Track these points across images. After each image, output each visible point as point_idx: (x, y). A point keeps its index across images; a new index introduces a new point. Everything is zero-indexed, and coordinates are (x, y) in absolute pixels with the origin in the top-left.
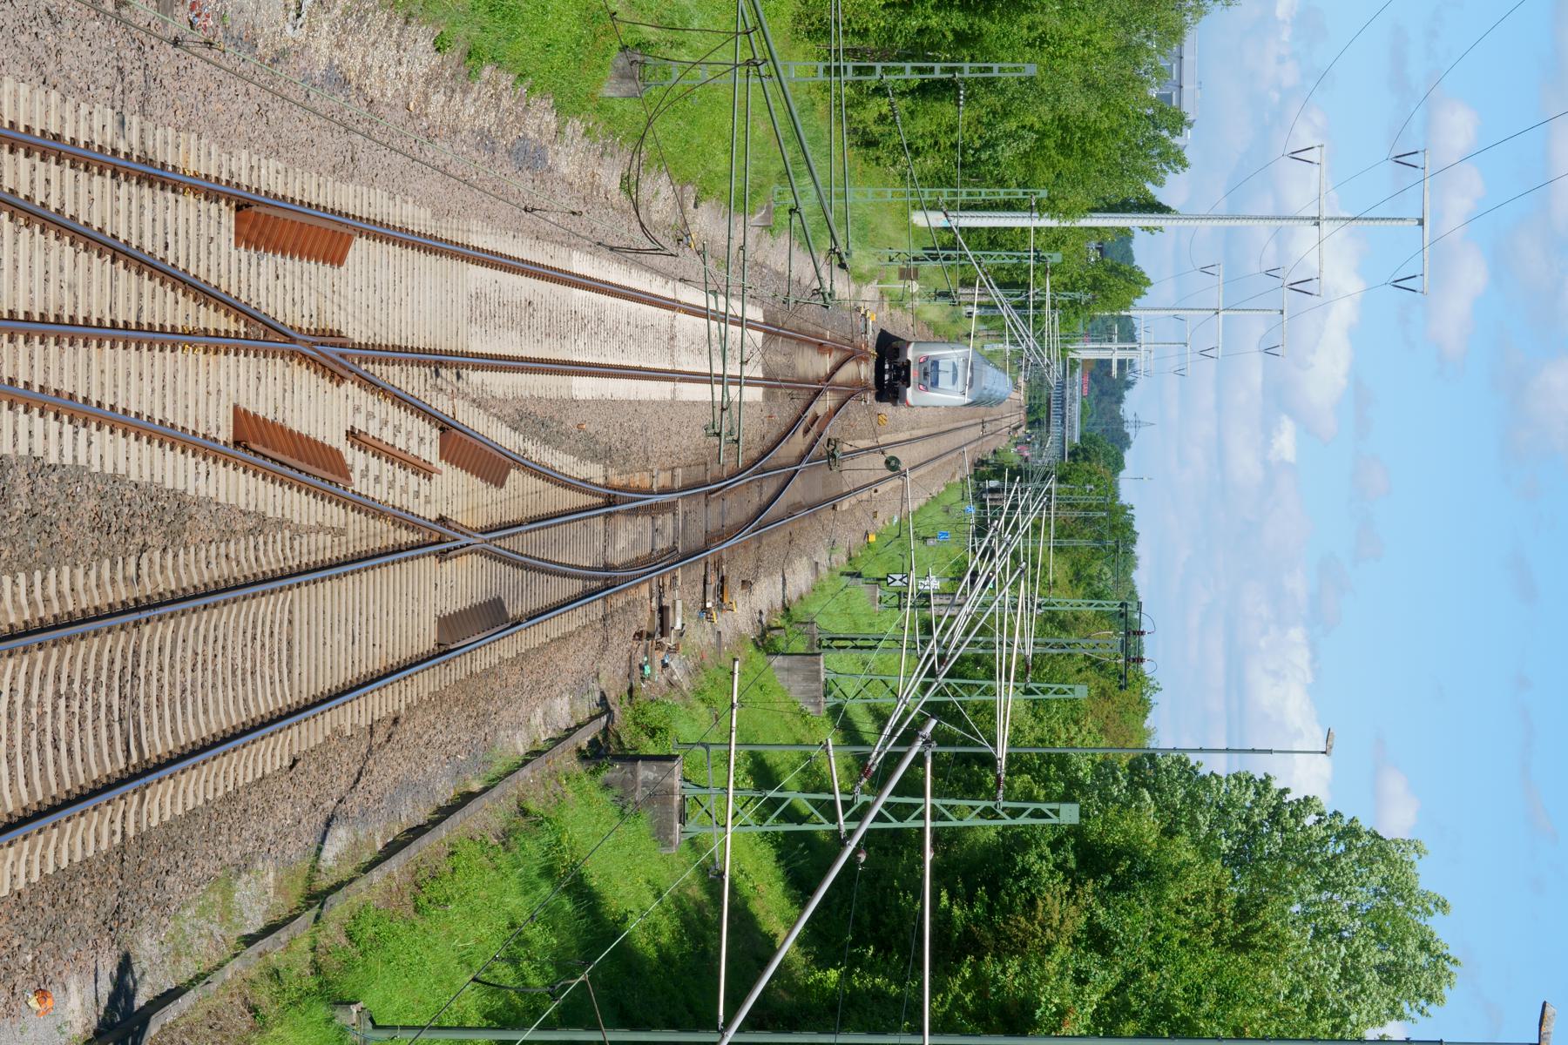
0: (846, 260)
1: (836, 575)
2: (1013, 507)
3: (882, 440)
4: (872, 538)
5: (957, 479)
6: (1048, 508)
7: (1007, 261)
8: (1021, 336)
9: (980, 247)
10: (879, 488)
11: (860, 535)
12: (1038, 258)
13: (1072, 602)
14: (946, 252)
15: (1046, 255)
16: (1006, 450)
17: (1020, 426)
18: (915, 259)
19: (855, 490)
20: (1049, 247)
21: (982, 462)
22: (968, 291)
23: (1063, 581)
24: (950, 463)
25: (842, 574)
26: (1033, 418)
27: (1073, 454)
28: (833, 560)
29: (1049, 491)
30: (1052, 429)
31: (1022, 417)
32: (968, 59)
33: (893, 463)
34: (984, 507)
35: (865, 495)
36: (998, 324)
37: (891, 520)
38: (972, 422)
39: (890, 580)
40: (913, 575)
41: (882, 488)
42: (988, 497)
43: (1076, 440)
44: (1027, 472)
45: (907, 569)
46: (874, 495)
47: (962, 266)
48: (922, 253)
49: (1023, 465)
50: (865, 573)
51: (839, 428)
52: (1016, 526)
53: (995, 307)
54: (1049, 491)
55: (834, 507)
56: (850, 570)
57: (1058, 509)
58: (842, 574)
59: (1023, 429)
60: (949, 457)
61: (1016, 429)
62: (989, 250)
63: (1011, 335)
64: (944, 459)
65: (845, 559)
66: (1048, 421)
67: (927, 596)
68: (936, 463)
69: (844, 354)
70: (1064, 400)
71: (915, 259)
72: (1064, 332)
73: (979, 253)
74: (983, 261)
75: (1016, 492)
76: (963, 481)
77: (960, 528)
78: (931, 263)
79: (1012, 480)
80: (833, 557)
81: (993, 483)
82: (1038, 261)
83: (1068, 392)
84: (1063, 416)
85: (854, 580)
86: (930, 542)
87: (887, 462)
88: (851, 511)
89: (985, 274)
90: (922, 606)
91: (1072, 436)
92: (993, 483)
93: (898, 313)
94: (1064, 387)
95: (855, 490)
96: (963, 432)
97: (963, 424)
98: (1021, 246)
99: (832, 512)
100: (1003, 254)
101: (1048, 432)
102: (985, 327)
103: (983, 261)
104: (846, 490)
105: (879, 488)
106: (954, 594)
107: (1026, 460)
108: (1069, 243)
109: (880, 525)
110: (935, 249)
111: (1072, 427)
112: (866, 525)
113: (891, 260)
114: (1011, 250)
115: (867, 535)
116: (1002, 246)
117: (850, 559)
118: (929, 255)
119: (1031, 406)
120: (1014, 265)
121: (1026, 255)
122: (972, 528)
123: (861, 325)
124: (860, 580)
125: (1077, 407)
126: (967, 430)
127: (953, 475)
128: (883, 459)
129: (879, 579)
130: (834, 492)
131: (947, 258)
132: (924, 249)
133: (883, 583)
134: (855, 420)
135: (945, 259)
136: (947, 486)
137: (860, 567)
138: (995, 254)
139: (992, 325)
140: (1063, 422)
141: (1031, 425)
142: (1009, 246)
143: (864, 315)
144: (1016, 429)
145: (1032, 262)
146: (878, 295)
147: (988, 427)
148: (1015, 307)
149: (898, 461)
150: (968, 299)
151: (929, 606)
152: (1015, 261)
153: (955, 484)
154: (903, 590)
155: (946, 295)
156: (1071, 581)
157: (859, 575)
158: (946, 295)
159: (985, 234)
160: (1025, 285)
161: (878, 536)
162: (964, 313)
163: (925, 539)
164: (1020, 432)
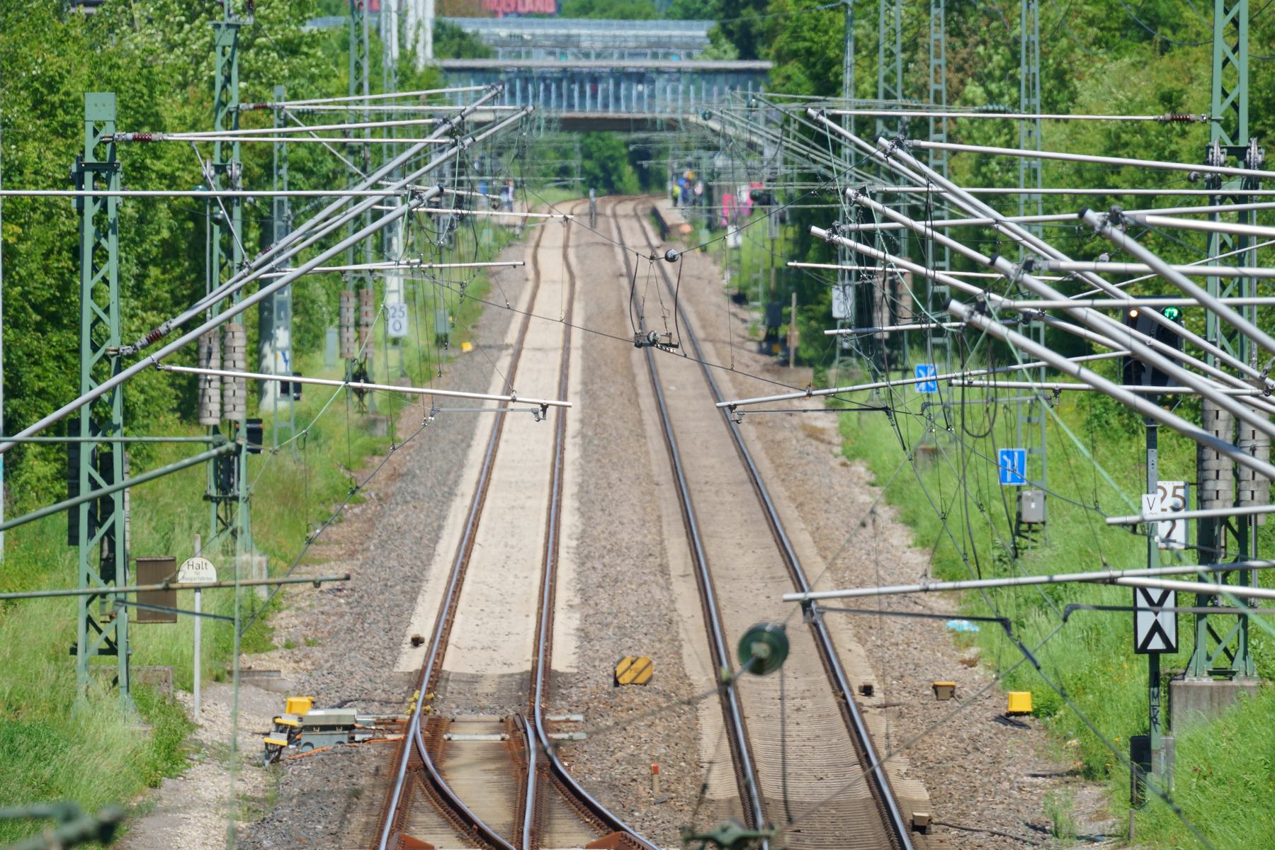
0: (87, 822)
1: (1141, 820)
2: (918, 248)
3: (702, 676)
4: (1021, 701)
5: (826, 422)
6: (920, 128)
7: (111, 268)
8: (359, 221)
9: (67, 359)
10: (857, 683)
11: (1012, 743)
12: (103, 171)
13: (1221, 47)
14: (86, 468)
15: (90, 143)
16: (735, 264)
17: (655, 215)
18: (108, 572)
19: (864, 759)
20: (67, 131)
21: (772, 342)
22: (213, 392)
23: (1162, 75)
24: (774, 447)
25: (1137, 802)
26: (628, 173)
27: (747, 46)
28: (1094, 829)
29: (862, 125)
30: (663, 110)
31: (626, 207)
32: (616, 56)
33: (760, 649)
34: (918, 339)
35: (878, 725)
36: (318, 291)
37: (962, 641)
38: (642, 377)
39: (1157, 643)
40: (1133, 575)
41: (859, 671)
42: (883, 328)
43: (699, 31)
44: (806, 197)
45: (1110, 596)
46: (878, 697)
47: (128, 414)
48: (89, 548)
49: (780, 207)
50: (1135, 728)
51: (663, 814)
52: (976, 236)
53: (264, 305)
54: (862, 125)
55: (920, 827)
56: (1123, 772)
57: (921, 91)
58: (1137, 802)
59: (664, 206)
60: (756, 449)
61: (664, 231)
62: (76, 326)
63: (356, 252)
64: (764, 466)
65: (1091, 792)
66: (640, 124)
67: (1207, 531)
68: (777, 491)
69: (420, 796)
70: (572, 76)
71: (108, 572)
72: (345, 76)
73: (89, 360)
74: (113, 344)
75: (869, 237)
76: (834, 405)
77: (977, 421)
78: (120, 516)
79: (830, 251)
80: (1084, 830)
81: (841, 304)
82: (111, 167)
83: (541, 61)
84: (622, 76)
85: (1159, 762)
86: (1033, 510)
87: (759, 667)
88: (930, 770)
89: (156, 338)
90: (1242, 537)
91: (689, 49)
92: (841, 304)
93: (285, 622)
94: (526, 76)
95: (864, 759)
96: (675, 404)
97: (647, 402)
98: (66, 224)
99: (936, 834)
100: (89, 282)
101: (672, 125)
102: (331, 335)
103: (113, 344)
104: (863, 791)
105: (857, 683)
106: (1201, 445)
107: (762, 199)
108: (55, 64)
109: (979, 672)
110: (74, 511)
111: (659, 48)
112: (980, 723)
113: (112, 649)
114: (76, 252)
115: (1010, 718)
116: (65, 287)
117: (1089, 773)
118: (94, 523)
119: (592, 182)
120: (128, 244)
121: (91, 210)
122: (977, 373)
123: (324, 742)
124: (1157, 741)
125: (589, 32)
126: (670, 390)
127: (815, 434)
128: (747, 681)
129: (1155, 679)
130: (871, 826)
131: (104, 464)
132: (74, 540)
133: (1167, 663)
134: (633, 759)
135: (107, 473)
136: (853, 454)
137: (1118, 735)
138: (88, 308)
139: (324, 309)
140: (640, 77)
141: (651, 181)
142: (66, 262)
143: (292, 734)
144: (664, 231)
145: (114, 192)
146: (225, 689)
147: (655, 326)
148: (264, 243)
149: (754, 634)
150: (238, 395)
151: (1244, 520)
152: (111, 244)
153: (842, 430)
154: (1189, 602)
155: (225, 466)
156: (1165, 47)
157: (1141, 750)
158: (225, 466)
159: (30, 339)
160: (196, 212)
161: (1014, 682)
162: (284, 404)
163: (1021, 527)
164: (672, 214)
